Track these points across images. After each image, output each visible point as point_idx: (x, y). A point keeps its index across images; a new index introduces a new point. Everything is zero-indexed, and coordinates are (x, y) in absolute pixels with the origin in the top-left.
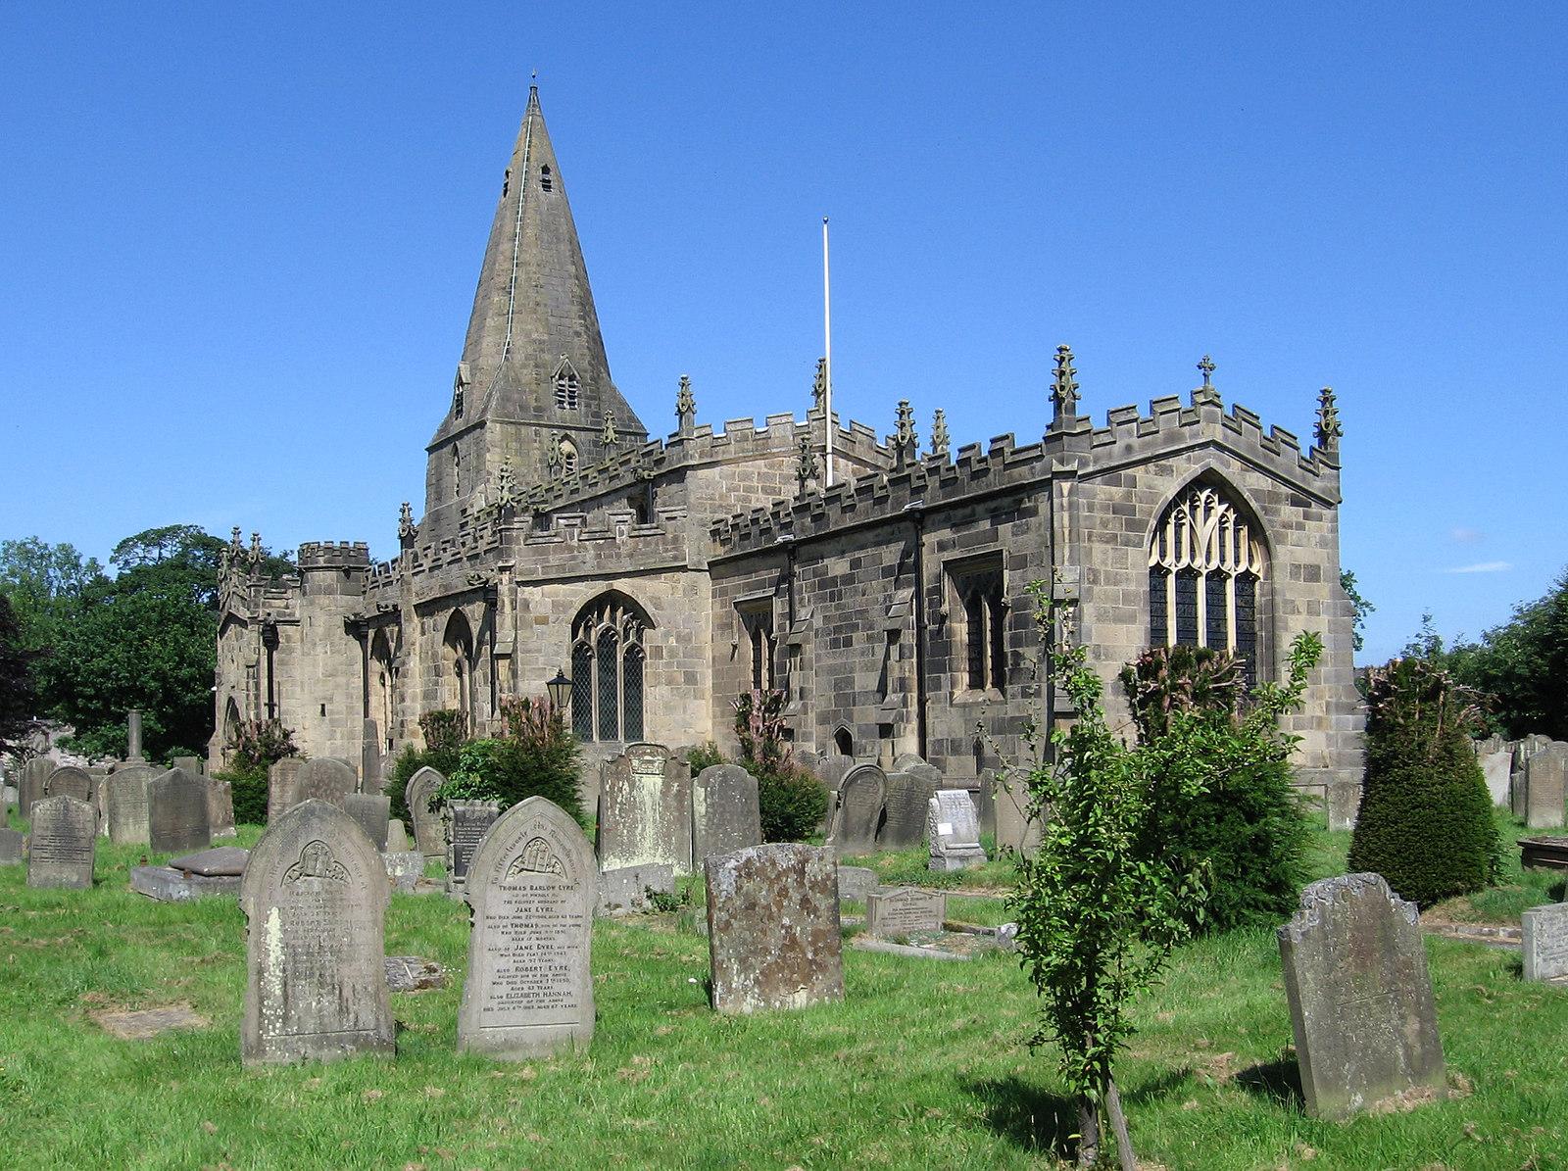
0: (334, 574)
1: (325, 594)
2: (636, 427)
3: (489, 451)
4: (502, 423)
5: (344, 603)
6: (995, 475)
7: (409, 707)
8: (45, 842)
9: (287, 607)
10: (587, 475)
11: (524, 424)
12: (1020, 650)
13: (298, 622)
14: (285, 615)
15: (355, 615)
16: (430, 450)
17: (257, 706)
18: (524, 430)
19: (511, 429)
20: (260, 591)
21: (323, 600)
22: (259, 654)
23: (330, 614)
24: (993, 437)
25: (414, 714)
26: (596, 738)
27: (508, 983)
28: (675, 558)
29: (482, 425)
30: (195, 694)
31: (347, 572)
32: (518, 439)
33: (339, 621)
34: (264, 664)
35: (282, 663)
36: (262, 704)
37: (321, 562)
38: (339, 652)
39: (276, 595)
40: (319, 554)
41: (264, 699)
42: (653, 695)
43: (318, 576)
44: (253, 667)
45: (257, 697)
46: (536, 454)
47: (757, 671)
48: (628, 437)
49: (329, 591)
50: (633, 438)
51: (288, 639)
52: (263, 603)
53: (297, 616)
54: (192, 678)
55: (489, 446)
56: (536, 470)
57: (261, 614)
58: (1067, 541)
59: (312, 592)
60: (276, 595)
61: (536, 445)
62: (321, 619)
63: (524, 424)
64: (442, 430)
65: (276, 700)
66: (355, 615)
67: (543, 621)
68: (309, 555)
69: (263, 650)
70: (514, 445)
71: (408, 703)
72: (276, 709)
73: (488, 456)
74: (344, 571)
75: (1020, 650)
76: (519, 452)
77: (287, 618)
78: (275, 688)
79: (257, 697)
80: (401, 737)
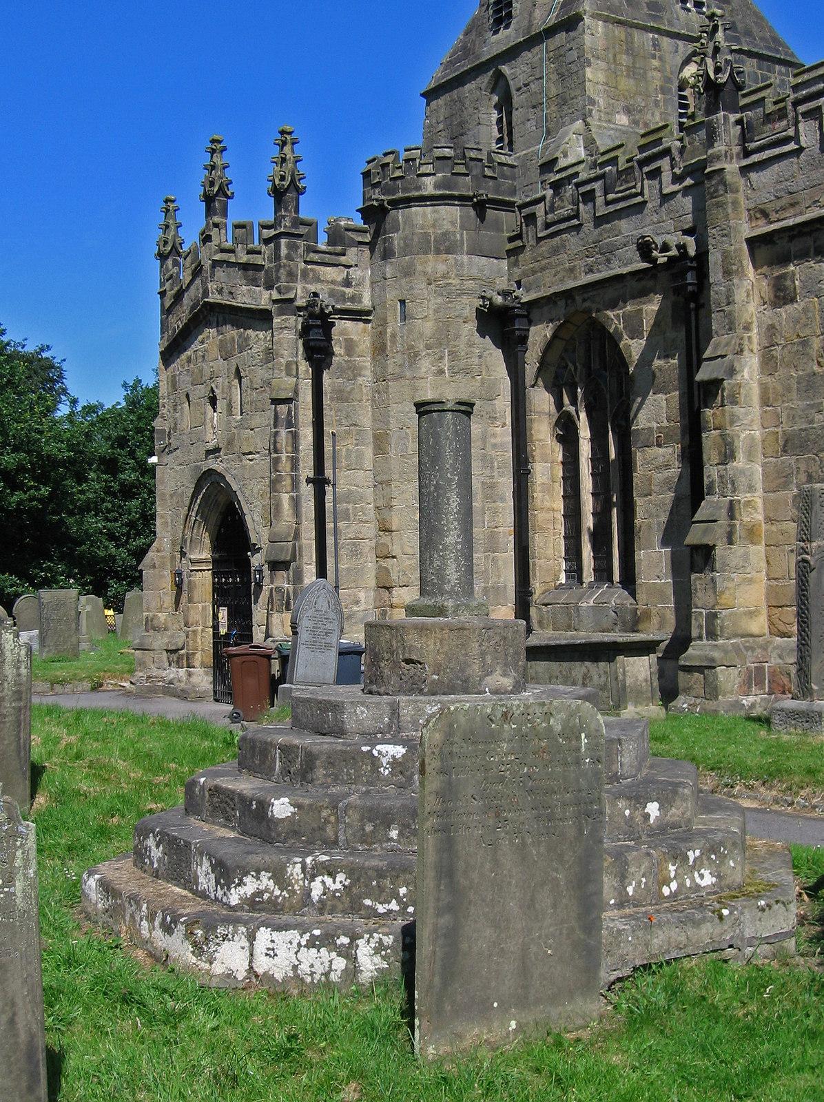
1: (438, 252)
2: (786, 54)
3: (589, 65)
4: (606, 20)
5: (475, 272)
7: (742, 472)
9: (347, 283)
10: (616, 157)
11: (637, 26)
13: (368, 313)
14: (343, 296)
17: (295, 485)
18: (637, 35)
19: (620, 32)
20: (297, 247)
21: (434, 264)
22: (297, 376)
23: (450, 294)
25: (751, 488)
29: (570, 23)
30: (25, 493)
31: (481, 207)
32: (630, 50)
33: (468, 306)
34: (306, 397)
35: (342, 396)
36: (303, 479)
37: (429, 186)
38: (467, 371)
39: (327, 258)
40: (424, 169)
41: (307, 470)
43: (421, 215)
44: (287, 401)
45: (295, 463)
46: (656, 79)
47: (573, 553)
48: (777, 67)
49: (446, 246)
50: (783, 69)
51: (350, 347)
52: (305, 274)
53: (366, 303)
54: (21, 469)
55: (589, 56)
56: (656, 103)
57: (300, 293)
59: (407, 249)
60: (327, 258)
61: (655, 63)
62: (427, 308)
63: (637, 26)
64: (465, 51)
65: (328, 472)
68: (398, 173)
69: (305, 368)
70: (624, 59)
71: (740, 462)
72: (329, 489)
73: (589, 73)
74: (475, 206)
76: (632, 72)
77: (349, 305)
78: (328, 448)
80: (731, 542)
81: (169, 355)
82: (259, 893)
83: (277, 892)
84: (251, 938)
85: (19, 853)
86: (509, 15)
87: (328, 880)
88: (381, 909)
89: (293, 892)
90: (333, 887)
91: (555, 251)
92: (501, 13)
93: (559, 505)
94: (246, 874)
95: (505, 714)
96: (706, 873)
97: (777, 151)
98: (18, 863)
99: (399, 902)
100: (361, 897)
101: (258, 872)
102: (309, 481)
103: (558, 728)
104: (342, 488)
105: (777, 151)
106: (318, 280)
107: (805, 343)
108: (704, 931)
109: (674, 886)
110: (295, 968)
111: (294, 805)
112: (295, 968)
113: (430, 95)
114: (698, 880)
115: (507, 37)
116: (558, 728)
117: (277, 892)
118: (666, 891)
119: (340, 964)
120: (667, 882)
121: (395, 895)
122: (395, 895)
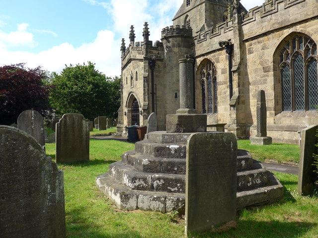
9: (158, 54)
35: (157, 76)
41: (150, 91)
65: (155, 91)
81: (123, 68)
82: (139, 185)
83: (144, 185)
84: (137, 197)
85: (57, 181)
86: (189, 3)
87: (158, 181)
88: (172, 190)
89: (148, 185)
90: (160, 184)
91: (201, 46)
92: (188, 4)
93: (201, 98)
94: (136, 179)
95: (211, 136)
96: (259, 180)
97: (249, 21)
98: (57, 184)
99: (178, 188)
100: (167, 186)
101: (139, 179)
102: (151, 93)
103: (225, 140)
104: (158, 95)
105: (249, 21)
106: (152, 53)
107: (255, 62)
108: (260, 197)
109: (251, 183)
110: (149, 207)
111: (149, 161)
112: (149, 207)
113: (173, 20)
114: (257, 182)
115: (190, 7)
116: (225, 140)
117: (144, 185)
118: (249, 185)
119: (162, 205)
120: (249, 182)
121: (177, 186)
122: (177, 186)
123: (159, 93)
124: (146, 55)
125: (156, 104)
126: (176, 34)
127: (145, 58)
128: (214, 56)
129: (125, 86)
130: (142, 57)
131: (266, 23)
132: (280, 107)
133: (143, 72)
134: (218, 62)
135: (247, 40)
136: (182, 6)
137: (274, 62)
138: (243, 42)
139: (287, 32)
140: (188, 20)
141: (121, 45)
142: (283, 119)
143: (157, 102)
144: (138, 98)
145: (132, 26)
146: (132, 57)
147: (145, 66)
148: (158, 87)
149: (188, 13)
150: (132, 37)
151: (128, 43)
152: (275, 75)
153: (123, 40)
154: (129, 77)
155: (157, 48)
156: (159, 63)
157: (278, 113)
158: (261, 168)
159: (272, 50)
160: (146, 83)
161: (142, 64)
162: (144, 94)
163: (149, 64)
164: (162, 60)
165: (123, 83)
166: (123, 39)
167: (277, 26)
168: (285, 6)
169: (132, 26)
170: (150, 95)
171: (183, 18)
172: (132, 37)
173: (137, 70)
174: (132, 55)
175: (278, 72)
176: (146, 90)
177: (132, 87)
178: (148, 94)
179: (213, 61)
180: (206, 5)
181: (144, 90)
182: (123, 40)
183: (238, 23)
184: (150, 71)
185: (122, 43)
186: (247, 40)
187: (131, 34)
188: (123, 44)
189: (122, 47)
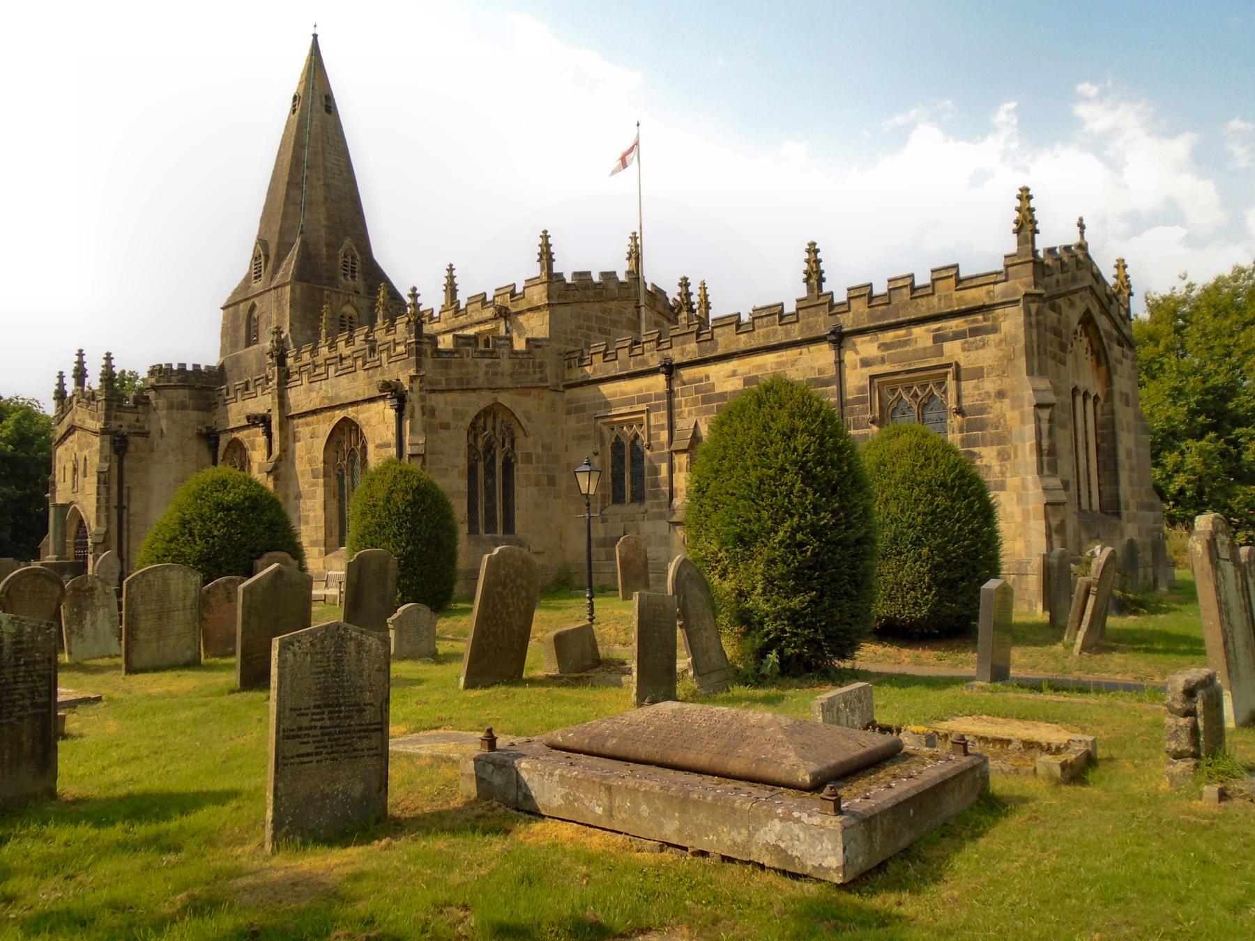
0: (187, 392)
1: (178, 409)
6: (940, 299)
8: (305, 722)
12: (976, 450)
14: (135, 427)
15: (207, 428)
16: (223, 308)
24: (850, 286)
26: (482, 530)
27: (314, 742)
28: (541, 380)
41: (114, 503)
42: (524, 494)
58: (1036, 353)
65: (125, 503)
66: (207, 428)
67: (446, 426)
75: (976, 450)
77: (138, 430)
79: (107, 500)
123: (135, 507)
124: (105, 424)
125: (128, 530)
126: (178, 381)
127: (104, 432)
128: (248, 437)
129: (59, 486)
130: (97, 425)
131: (314, 394)
132: (335, 539)
133: (97, 459)
134: (254, 449)
135: (292, 417)
136: (247, 280)
137: (325, 462)
138: (286, 419)
139: (339, 415)
140: (256, 314)
141: (56, 388)
142: (334, 561)
143: (131, 527)
144: (87, 517)
145: (81, 351)
146: (78, 423)
147: (102, 447)
148: (135, 494)
149: (256, 301)
150: (80, 374)
151: (70, 386)
152: (325, 485)
153: (61, 376)
154: (70, 466)
155: (136, 407)
156: (139, 440)
157: (332, 551)
158: (467, 687)
159: (321, 442)
160: (102, 486)
161: (97, 440)
162: (98, 509)
163: (113, 443)
164: (145, 434)
165: (57, 478)
166: (61, 373)
167: (327, 404)
168: (336, 372)
169: (81, 351)
170: (114, 512)
171: (243, 308)
172: (80, 374)
173: (86, 452)
174: (77, 418)
175: (334, 481)
176: (103, 501)
177: (75, 489)
178: (108, 509)
179: (247, 445)
180: (292, 290)
181: (98, 500)
182: (61, 376)
183: (279, 384)
184: (115, 458)
185: (57, 381)
186: (292, 417)
187: (76, 370)
188: (61, 385)
189: (56, 392)
